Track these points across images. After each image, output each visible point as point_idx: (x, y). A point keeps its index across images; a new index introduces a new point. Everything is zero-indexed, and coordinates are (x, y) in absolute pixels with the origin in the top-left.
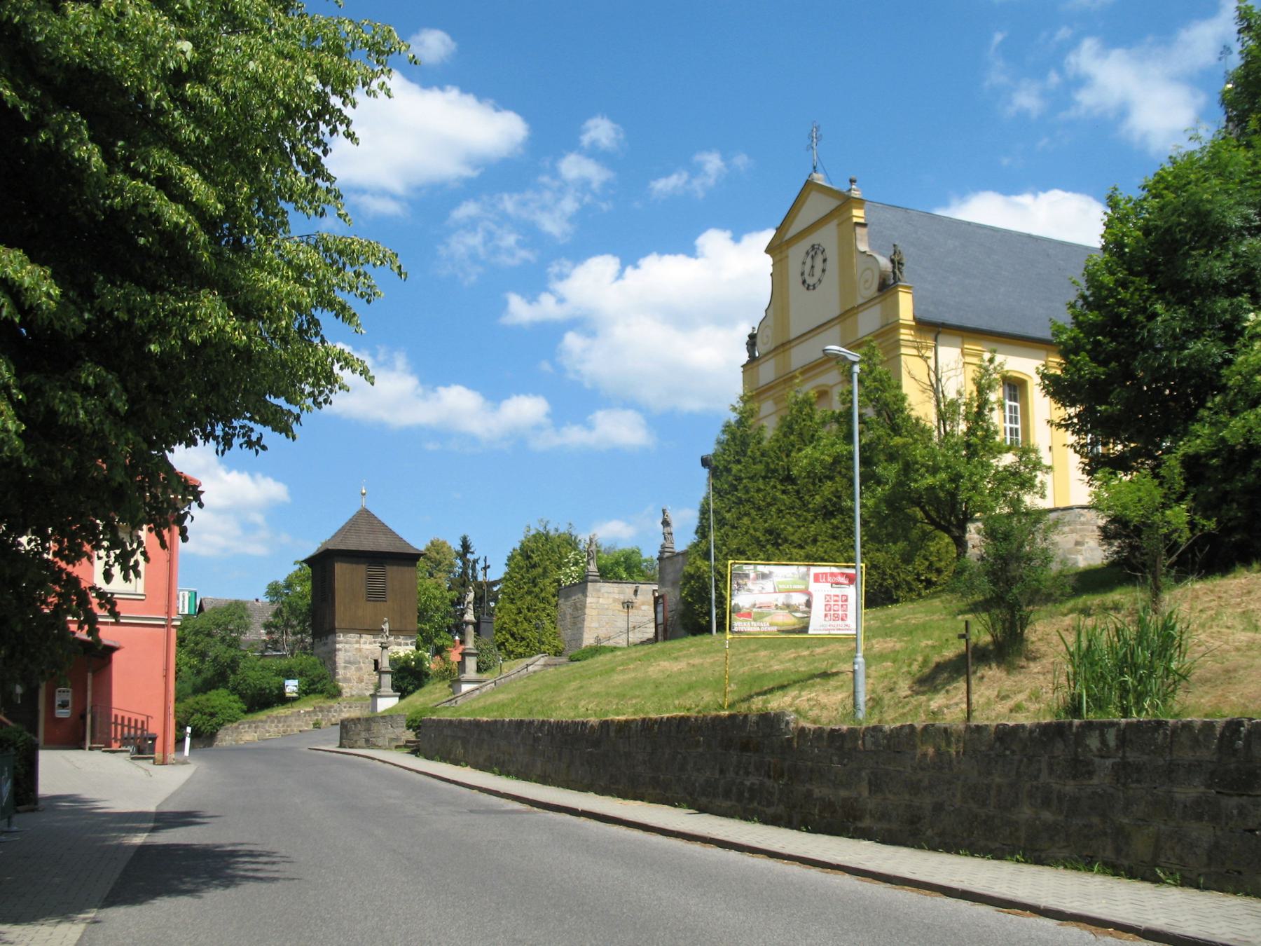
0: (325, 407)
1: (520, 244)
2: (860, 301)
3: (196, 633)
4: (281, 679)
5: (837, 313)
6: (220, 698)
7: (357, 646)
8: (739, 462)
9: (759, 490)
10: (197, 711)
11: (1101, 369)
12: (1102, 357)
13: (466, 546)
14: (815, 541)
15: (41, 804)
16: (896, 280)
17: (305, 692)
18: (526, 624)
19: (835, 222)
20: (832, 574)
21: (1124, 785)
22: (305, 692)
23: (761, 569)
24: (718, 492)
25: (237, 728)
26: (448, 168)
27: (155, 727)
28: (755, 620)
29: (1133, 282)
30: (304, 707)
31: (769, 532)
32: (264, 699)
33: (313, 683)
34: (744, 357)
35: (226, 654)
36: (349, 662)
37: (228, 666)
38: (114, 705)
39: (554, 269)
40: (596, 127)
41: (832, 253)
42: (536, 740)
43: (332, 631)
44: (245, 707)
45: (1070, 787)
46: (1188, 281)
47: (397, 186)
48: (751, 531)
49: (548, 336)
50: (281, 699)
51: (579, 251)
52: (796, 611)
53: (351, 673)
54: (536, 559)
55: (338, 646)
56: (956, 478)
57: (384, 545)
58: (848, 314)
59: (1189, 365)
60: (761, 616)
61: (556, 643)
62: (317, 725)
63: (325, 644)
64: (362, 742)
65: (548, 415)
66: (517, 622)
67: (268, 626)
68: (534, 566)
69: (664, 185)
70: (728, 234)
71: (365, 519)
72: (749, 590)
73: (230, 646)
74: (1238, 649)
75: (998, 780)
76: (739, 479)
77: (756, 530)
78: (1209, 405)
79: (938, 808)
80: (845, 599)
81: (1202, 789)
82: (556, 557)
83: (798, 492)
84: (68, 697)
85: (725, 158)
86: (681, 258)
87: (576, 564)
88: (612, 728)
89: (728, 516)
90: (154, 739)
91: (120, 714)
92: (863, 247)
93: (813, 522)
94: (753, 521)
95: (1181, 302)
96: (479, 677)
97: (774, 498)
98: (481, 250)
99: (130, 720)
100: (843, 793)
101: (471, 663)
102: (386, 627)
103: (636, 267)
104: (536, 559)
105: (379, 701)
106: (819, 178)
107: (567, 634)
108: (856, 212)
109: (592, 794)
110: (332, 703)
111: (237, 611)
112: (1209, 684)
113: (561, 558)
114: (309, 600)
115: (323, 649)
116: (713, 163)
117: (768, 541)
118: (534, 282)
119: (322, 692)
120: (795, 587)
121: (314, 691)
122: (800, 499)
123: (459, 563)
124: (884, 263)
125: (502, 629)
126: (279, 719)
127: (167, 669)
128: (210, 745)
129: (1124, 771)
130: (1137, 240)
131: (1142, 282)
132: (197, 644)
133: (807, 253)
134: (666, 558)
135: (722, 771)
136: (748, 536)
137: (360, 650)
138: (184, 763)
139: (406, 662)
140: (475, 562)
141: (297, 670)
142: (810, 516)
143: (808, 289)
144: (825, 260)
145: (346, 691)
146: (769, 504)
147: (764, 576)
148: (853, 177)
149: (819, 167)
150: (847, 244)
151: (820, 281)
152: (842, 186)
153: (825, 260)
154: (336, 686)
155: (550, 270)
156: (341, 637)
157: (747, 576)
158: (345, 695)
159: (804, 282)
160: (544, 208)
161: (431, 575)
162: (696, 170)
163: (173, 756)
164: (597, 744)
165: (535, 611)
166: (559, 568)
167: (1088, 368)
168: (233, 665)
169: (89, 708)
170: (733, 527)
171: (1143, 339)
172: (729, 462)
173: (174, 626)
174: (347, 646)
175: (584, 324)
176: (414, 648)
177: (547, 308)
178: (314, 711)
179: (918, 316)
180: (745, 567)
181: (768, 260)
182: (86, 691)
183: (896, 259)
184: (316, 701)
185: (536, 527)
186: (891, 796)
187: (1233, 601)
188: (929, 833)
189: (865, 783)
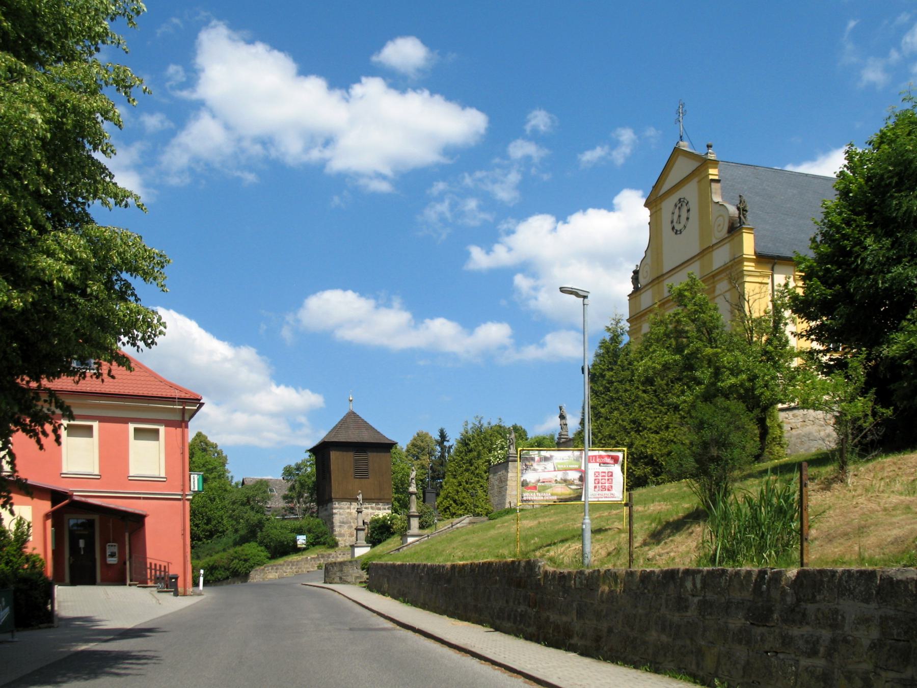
0: (153, 347)
1: (481, 208)
2: (714, 241)
3: (234, 503)
4: (294, 535)
5: (698, 251)
6: (252, 549)
8: (612, 369)
9: (626, 391)
10: (236, 558)
11: (829, 291)
12: (830, 281)
13: (443, 436)
14: (667, 428)
15: (56, 623)
16: (742, 223)
17: (311, 544)
18: (464, 493)
19: (696, 180)
20: (601, 457)
21: (703, 616)
22: (311, 544)
23: (543, 453)
24: (594, 392)
26: (423, 154)
27: (175, 569)
28: (539, 492)
29: (855, 221)
30: (311, 555)
31: (633, 422)
32: (283, 549)
33: (318, 538)
34: (630, 288)
35: (254, 517)
37: (257, 526)
38: (148, 556)
39: (504, 226)
40: (536, 117)
41: (694, 205)
42: (421, 578)
43: (330, 500)
44: (269, 555)
45: (676, 618)
46: (896, 217)
47: (387, 171)
48: (620, 422)
49: (502, 278)
50: (294, 549)
51: (522, 212)
52: (572, 484)
53: (345, 530)
54: (472, 445)
55: (334, 511)
56: (753, 378)
57: (366, 437)
58: (705, 252)
59: (891, 286)
60: (544, 489)
61: (487, 506)
63: (326, 510)
64: (337, 579)
65: (511, 337)
66: (458, 492)
67: (285, 497)
68: (470, 451)
69: (591, 156)
71: (352, 418)
72: (534, 470)
73: (257, 512)
74: (885, 510)
75: (641, 611)
76: (611, 382)
77: (623, 421)
78: (909, 317)
79: (610, 630)
80: (611, 474)
81: (743, 621)
82: (489, 443)
83: (655, 391)
84: (115, 550)
85: (637, 132)
86: (603, 212)
87: (502, 448)
88: (67, 579)
89: (602, 410)
90: (176, 578)
91: (153, 562)
92: (717, 198)
93: (666, 414)
94: (621, 414)
95: (888, 234)
96: (421, 532)
97: (637, 397)
98: (448, 215)
99: (156, 565)
100: (564, 619)
101: (415, 523)
102: (360, 497)
103: (565, 222)
104: (472, 445)
105: (356, 550)
106: (685, 146)
107: (494, 500)
108: (711, 171)
109: (445, 617)
110: (331, 551)
111: (263, 486)
112: (846, 537)
113: (492, 444)
114: (314, 479)
115: (325, 513)
116: (626, 135)
117: (632, 428)
118: (489, 237)
119: (324, 544)
120: (571, 466)
121: (318, 543)
122: (657, 396)
123: (439, 448)
124: (733, 210)
125: (446, 497)
126: (292, 563)
127: (184, 530)
128: (246, 581)
129: (705, 606)
130: (860, 187)
131: (862, 220)
132: (234, 511)
133: (676, 205)
135: (507, 602)
136: (617, 425)
138: (200, 594)
139: (384, 522)
140: (450, 447)
141: (305, 529)
142: (663, 409)
143: (676, 233)
144: (688, 211)
146: (634, 401)
147: (546, 459)
148: (710, 143)
149: (684, 136)
150: (705, 196)
151: (685, 227)
152: (700, 151)
153: (688, 211)
154: (334, 540)
155: (499, 227)
156: (336, 505)
157: (533, 459)
158: (340, 546)
159: (673, 228)
160: (495, 181)
161: (418, 458)
162: (615, 144)
163: (191, 590)
164: (449, 581)
165: (471, 483)
166: (490, 451)
167: (822, 291)
168: (260, 525)
169: (127, 557)
170: (606, 419)
171: (857, 265)
172: (604, 370)
173: (188, 500)
174: (341, 511)
175: (527, 267)
176: (390, 512)
177: (501, 256)
178: (318, 558)
179: (758, 251)
180: (531, 453)
181: (646, 213)
182: (125, 546)
183: (741, 207)
184: (320, 550)
185: (472, 422)
186: (587, 622)
187: (908, 471)
188: (605, 649)
189: (574, 612)
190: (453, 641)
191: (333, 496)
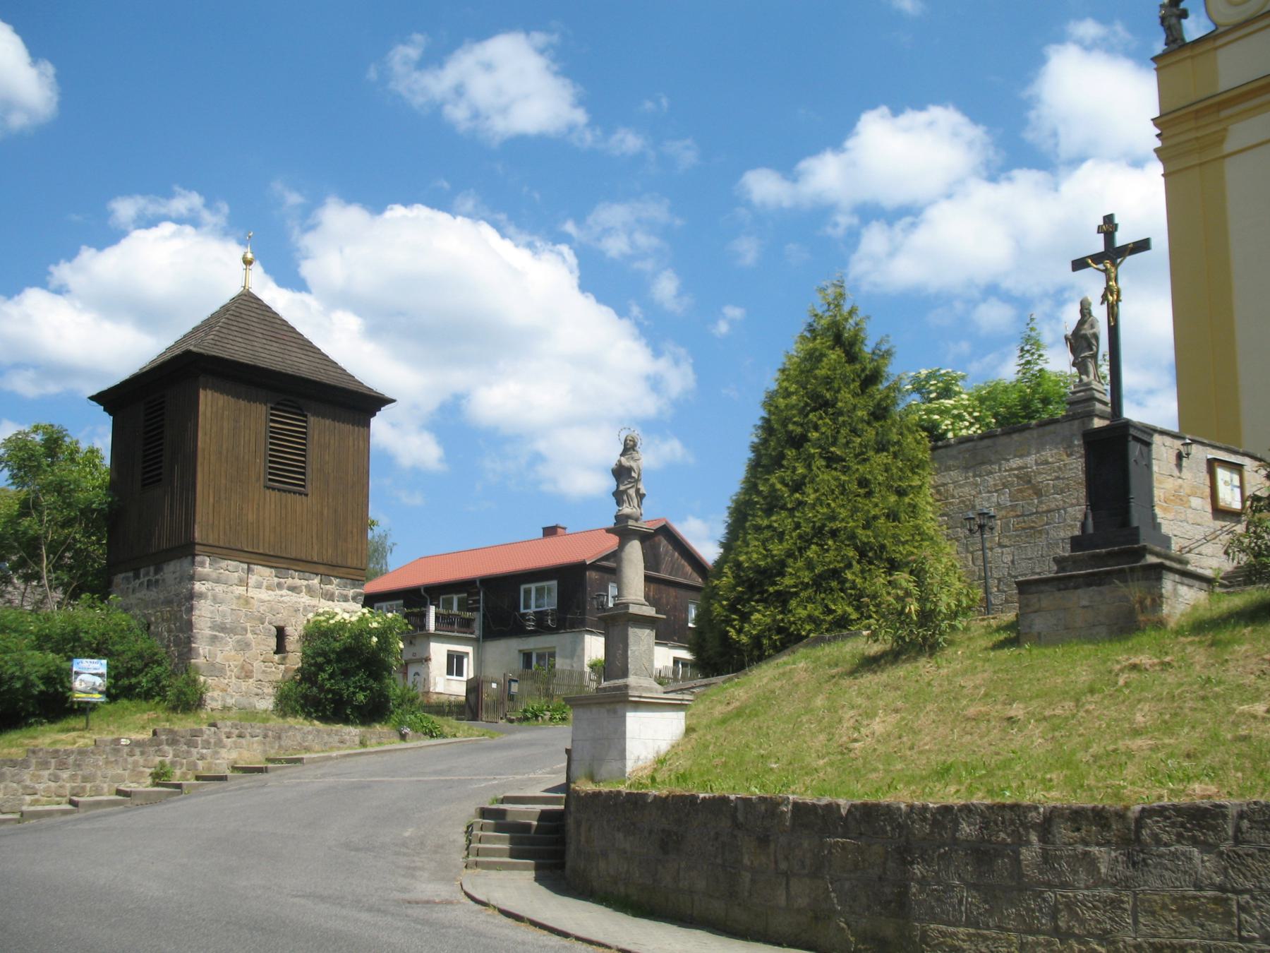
7: (241, 590)
22: (121, 689)
36: (223, 628)
43: (186, 549)
50: (56, 705)
55: (198, 587)
70: (884, 110)
110: (183, 724)
119: (147, 695)
126: (61, 759)
134: (626, 606)
137: (247, 601)
145: (214, 699)
156: (205, 567)
174: (219, 588)
184: (134, 725)
190: (1255, 142)
191: (197, 536)
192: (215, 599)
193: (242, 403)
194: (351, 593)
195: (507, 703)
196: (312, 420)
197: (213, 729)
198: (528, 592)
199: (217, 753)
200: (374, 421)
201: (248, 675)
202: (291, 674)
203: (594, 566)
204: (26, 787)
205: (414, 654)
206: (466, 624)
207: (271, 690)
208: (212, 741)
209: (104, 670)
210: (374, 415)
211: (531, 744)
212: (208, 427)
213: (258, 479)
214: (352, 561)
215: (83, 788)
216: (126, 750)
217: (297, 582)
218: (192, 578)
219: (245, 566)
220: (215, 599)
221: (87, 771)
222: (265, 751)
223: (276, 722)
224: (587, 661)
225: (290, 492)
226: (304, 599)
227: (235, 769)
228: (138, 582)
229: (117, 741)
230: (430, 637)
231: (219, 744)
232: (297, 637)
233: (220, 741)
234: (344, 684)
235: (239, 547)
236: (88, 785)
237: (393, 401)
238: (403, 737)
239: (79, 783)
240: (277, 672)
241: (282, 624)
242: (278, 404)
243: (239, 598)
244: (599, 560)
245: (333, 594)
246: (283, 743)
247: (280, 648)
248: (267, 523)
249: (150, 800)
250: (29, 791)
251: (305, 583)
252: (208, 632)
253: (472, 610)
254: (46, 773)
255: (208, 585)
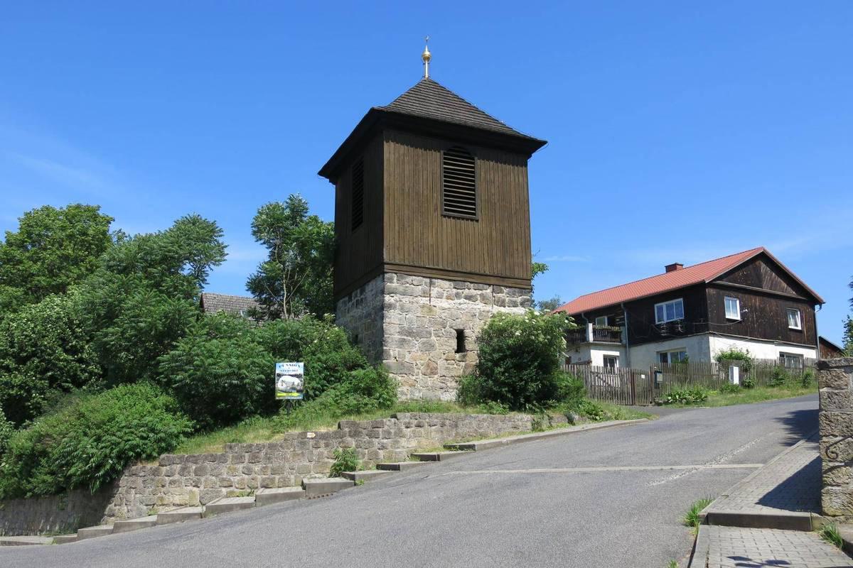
7: (424, 300)
25: (155, 472)
36: (410, 333)
43: (376, 269)
50: (268, 404)
62: (344, 468)
137: (431, 309)
156: (393, 282)
174: (406, 299)
191: (386, 258)
192: (402, 309)
193: (420, 151)
194: (519, 299)
195: (654, 390)
196: (478, 162)
197: (393, 420)
198: (660, 309)
199: (397, 442)
200: (531, 162)
201: (434, 372)
202: (469, 370)
203: (712, 285)
204: (223, 480)
205: (580, 359)
206: (615, 336)
207: (454, 384)
208: (392, 431)
209: (301, 371)
210: (530, 156)
211: (690, 425)
212: (392, 169)
213: (436, 210)
214: (518, 273)
215: (273, 480)
216: (312, 443)
217: (473, 292)
218: (383, 292)
219: (428, 280)
220: (402, 309)
221: (275, 465)
222: (443, 439)
223: (457, 412)
224: (712, 354)
225: (463, 219)
226: (479, 306)
227: (413, 456)
228: (351, 303)
229: (304, 435)
230: (590, 346)
231: (400, 434)
232: (474, 338)
233: (400, 430)
234: (518, 374)
235: (422, 265)
236: (277, 477)
237: (545, 143)
238: (571, 421)
239: (269, 475)
240: (459, 369)
241: (461, 327)
242: (450, 150)
243: (423, 307)
244: (714, 280)
245: (503, 301)
246: (460, 431)
247: (461, 348)
248: (445, 244)
249: (325, 492)
250: (225, 483)
251: (480, 292)
252: (397, 337)
253: (619, 326)
254: (240, 466)
255: (397, 297)
